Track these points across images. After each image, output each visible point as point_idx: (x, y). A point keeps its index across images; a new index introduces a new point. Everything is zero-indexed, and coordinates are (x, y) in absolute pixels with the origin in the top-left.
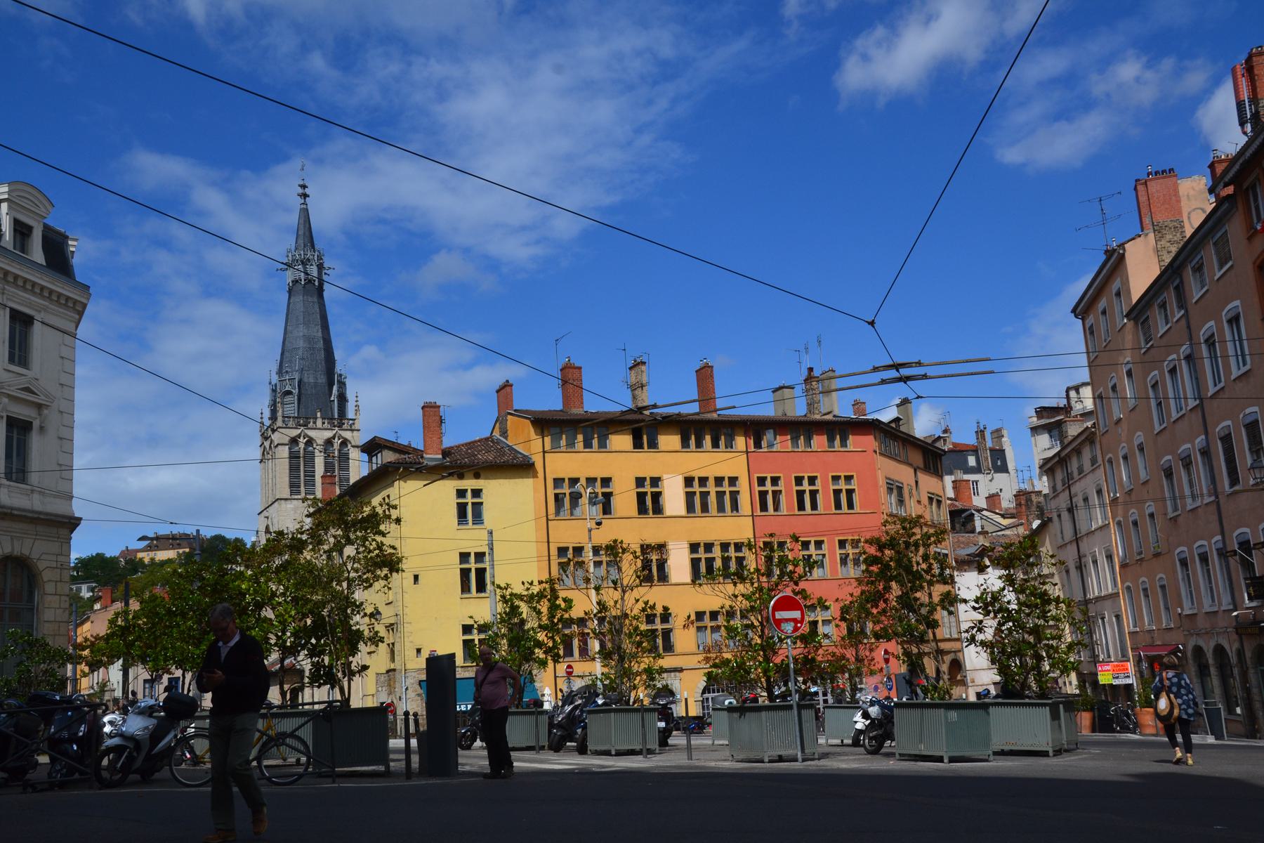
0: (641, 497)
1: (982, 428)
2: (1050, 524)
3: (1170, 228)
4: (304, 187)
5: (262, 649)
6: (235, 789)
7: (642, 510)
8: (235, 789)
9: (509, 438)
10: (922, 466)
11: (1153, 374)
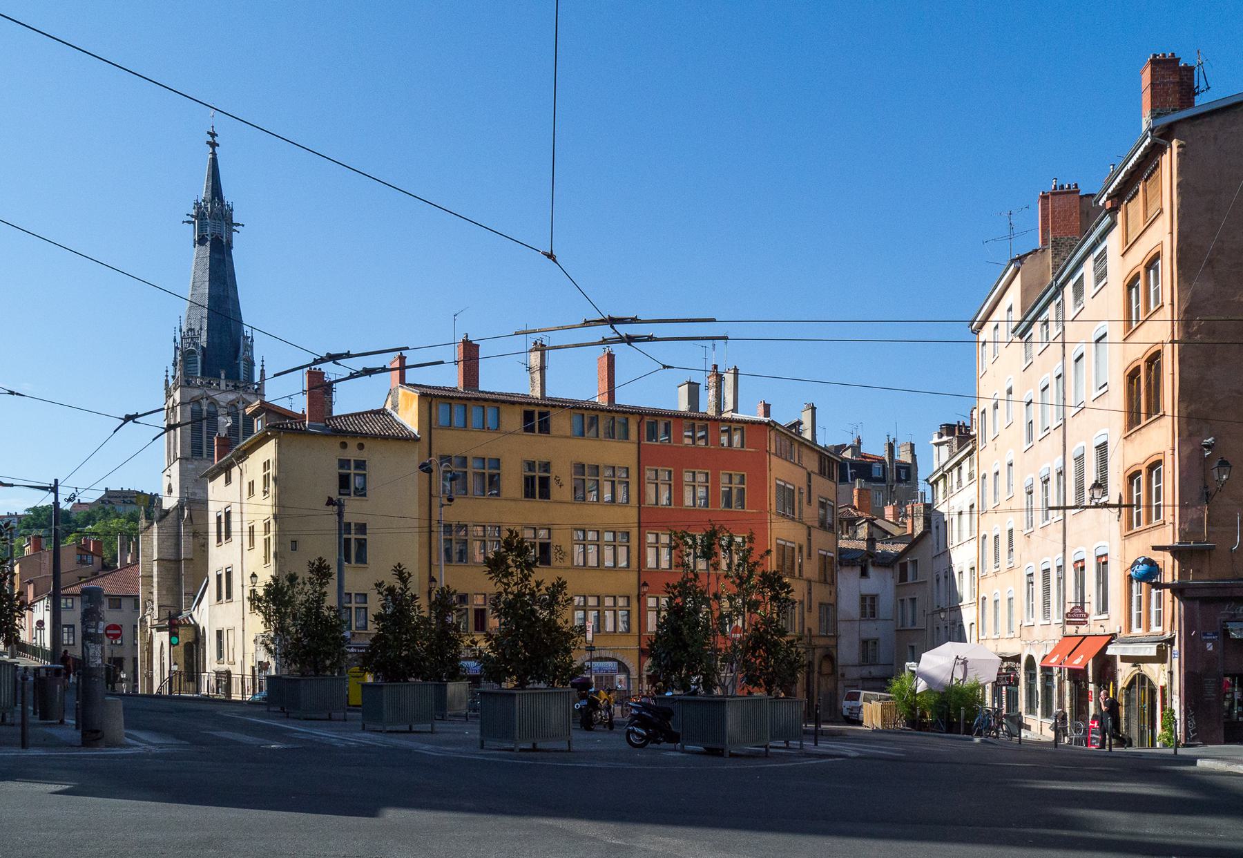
0: (529, 481)
1: (891, 441)
2: (929, 534)
3: (1067, 246)
4: (213, 135)
5: (60, 603)
6: (668, 694)
7: (529, 494)
8: (668, 694)
9: (399, 412)
10: (816, 471)
11: (1028, 392)
